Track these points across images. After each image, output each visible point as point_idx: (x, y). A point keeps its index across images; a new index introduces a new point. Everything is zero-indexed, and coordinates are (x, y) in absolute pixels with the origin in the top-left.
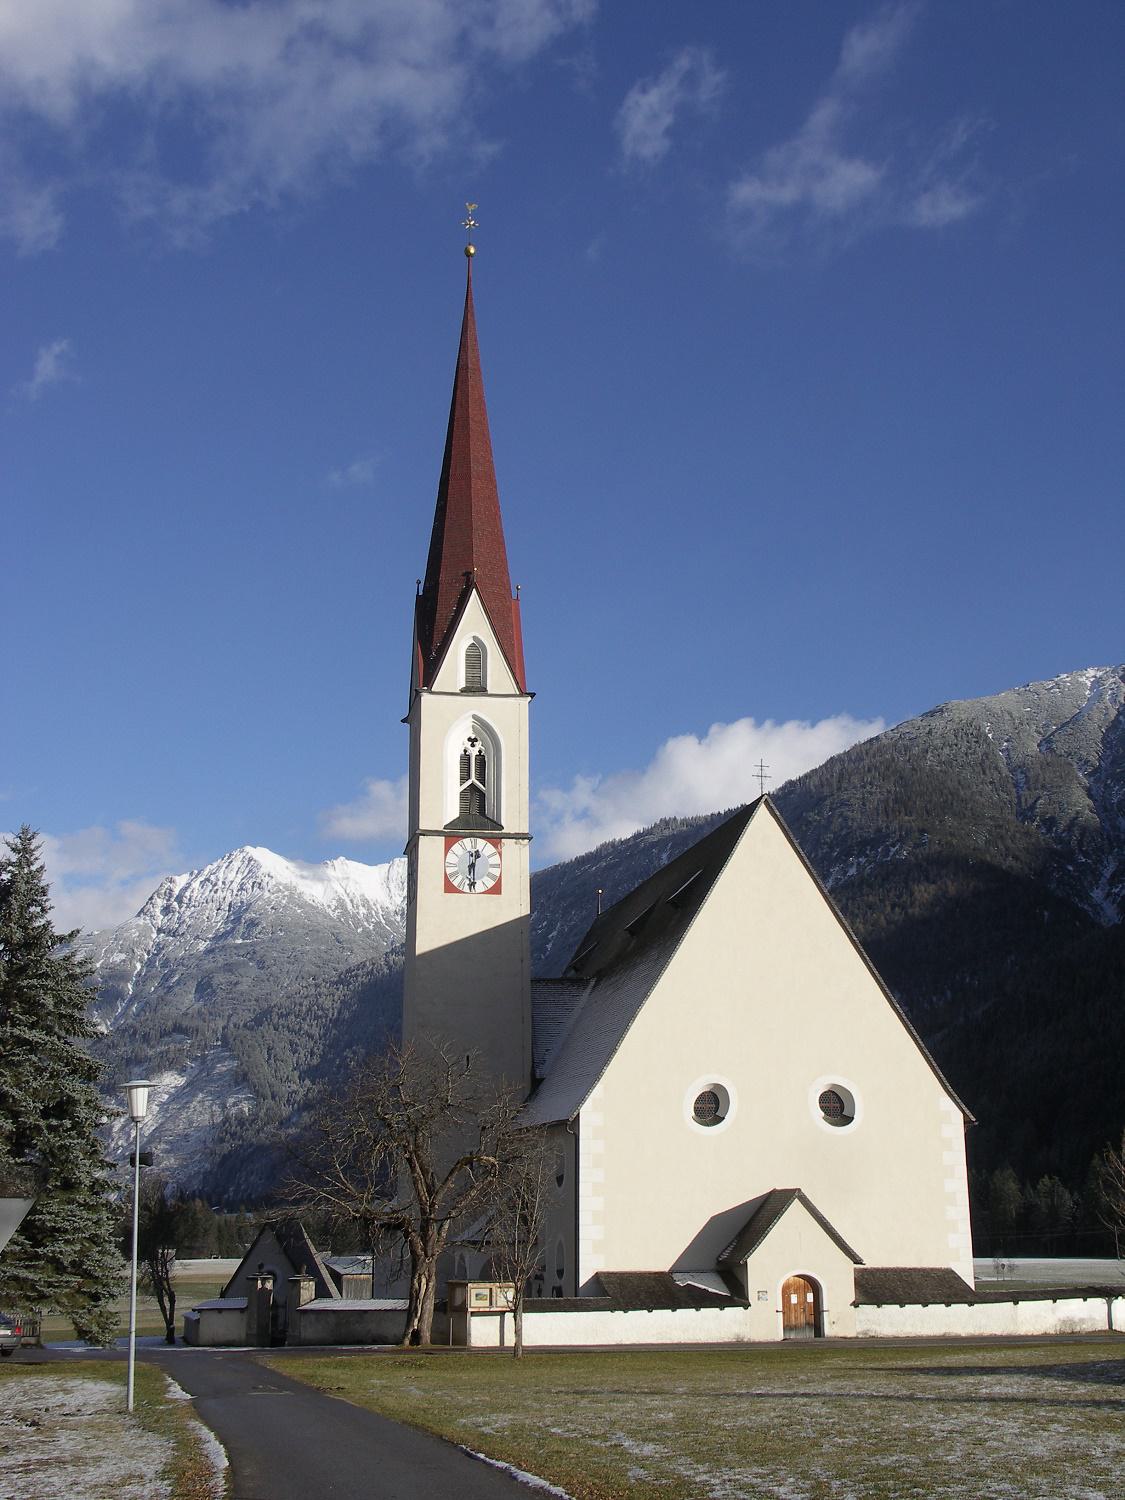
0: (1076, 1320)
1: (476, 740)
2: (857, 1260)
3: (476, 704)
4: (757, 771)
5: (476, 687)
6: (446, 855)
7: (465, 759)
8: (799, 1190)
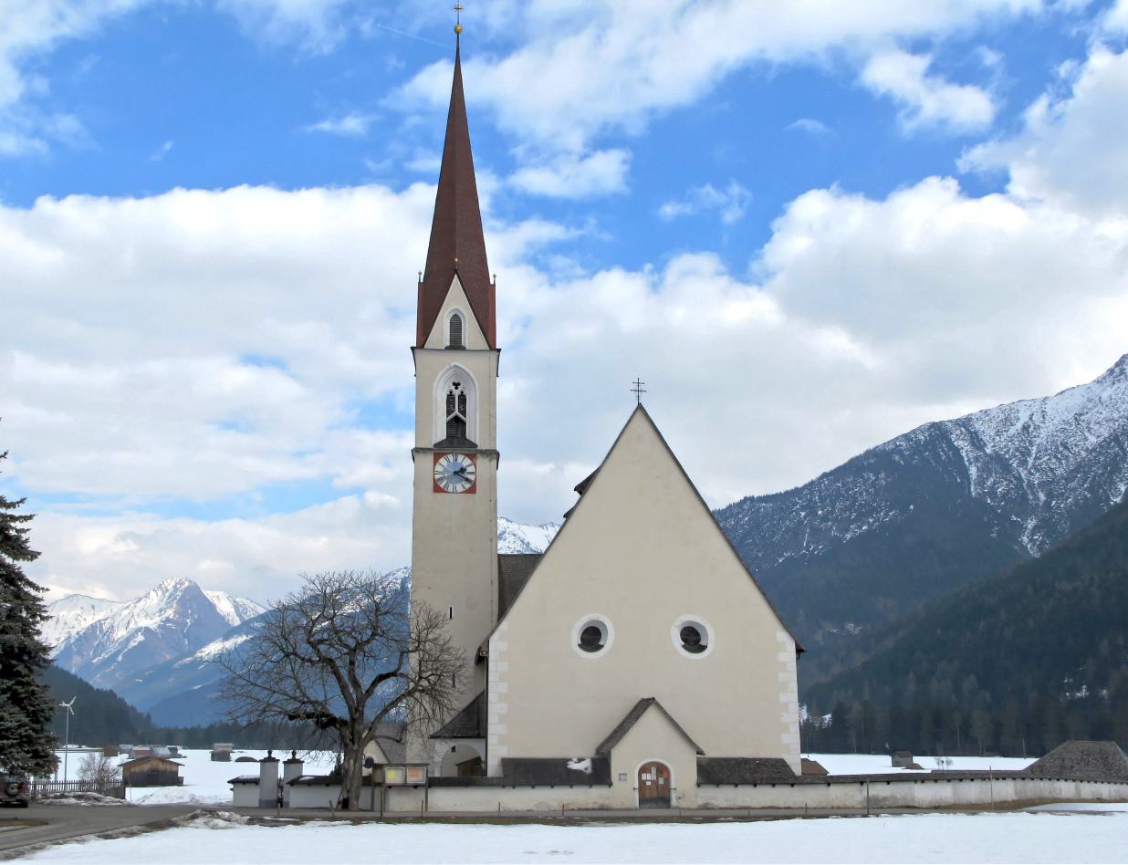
0: (880, 797)
2: (700, 752)
3: (457, 359)
4: (635, 387)
7: (450, 397)
8: (653, 699)
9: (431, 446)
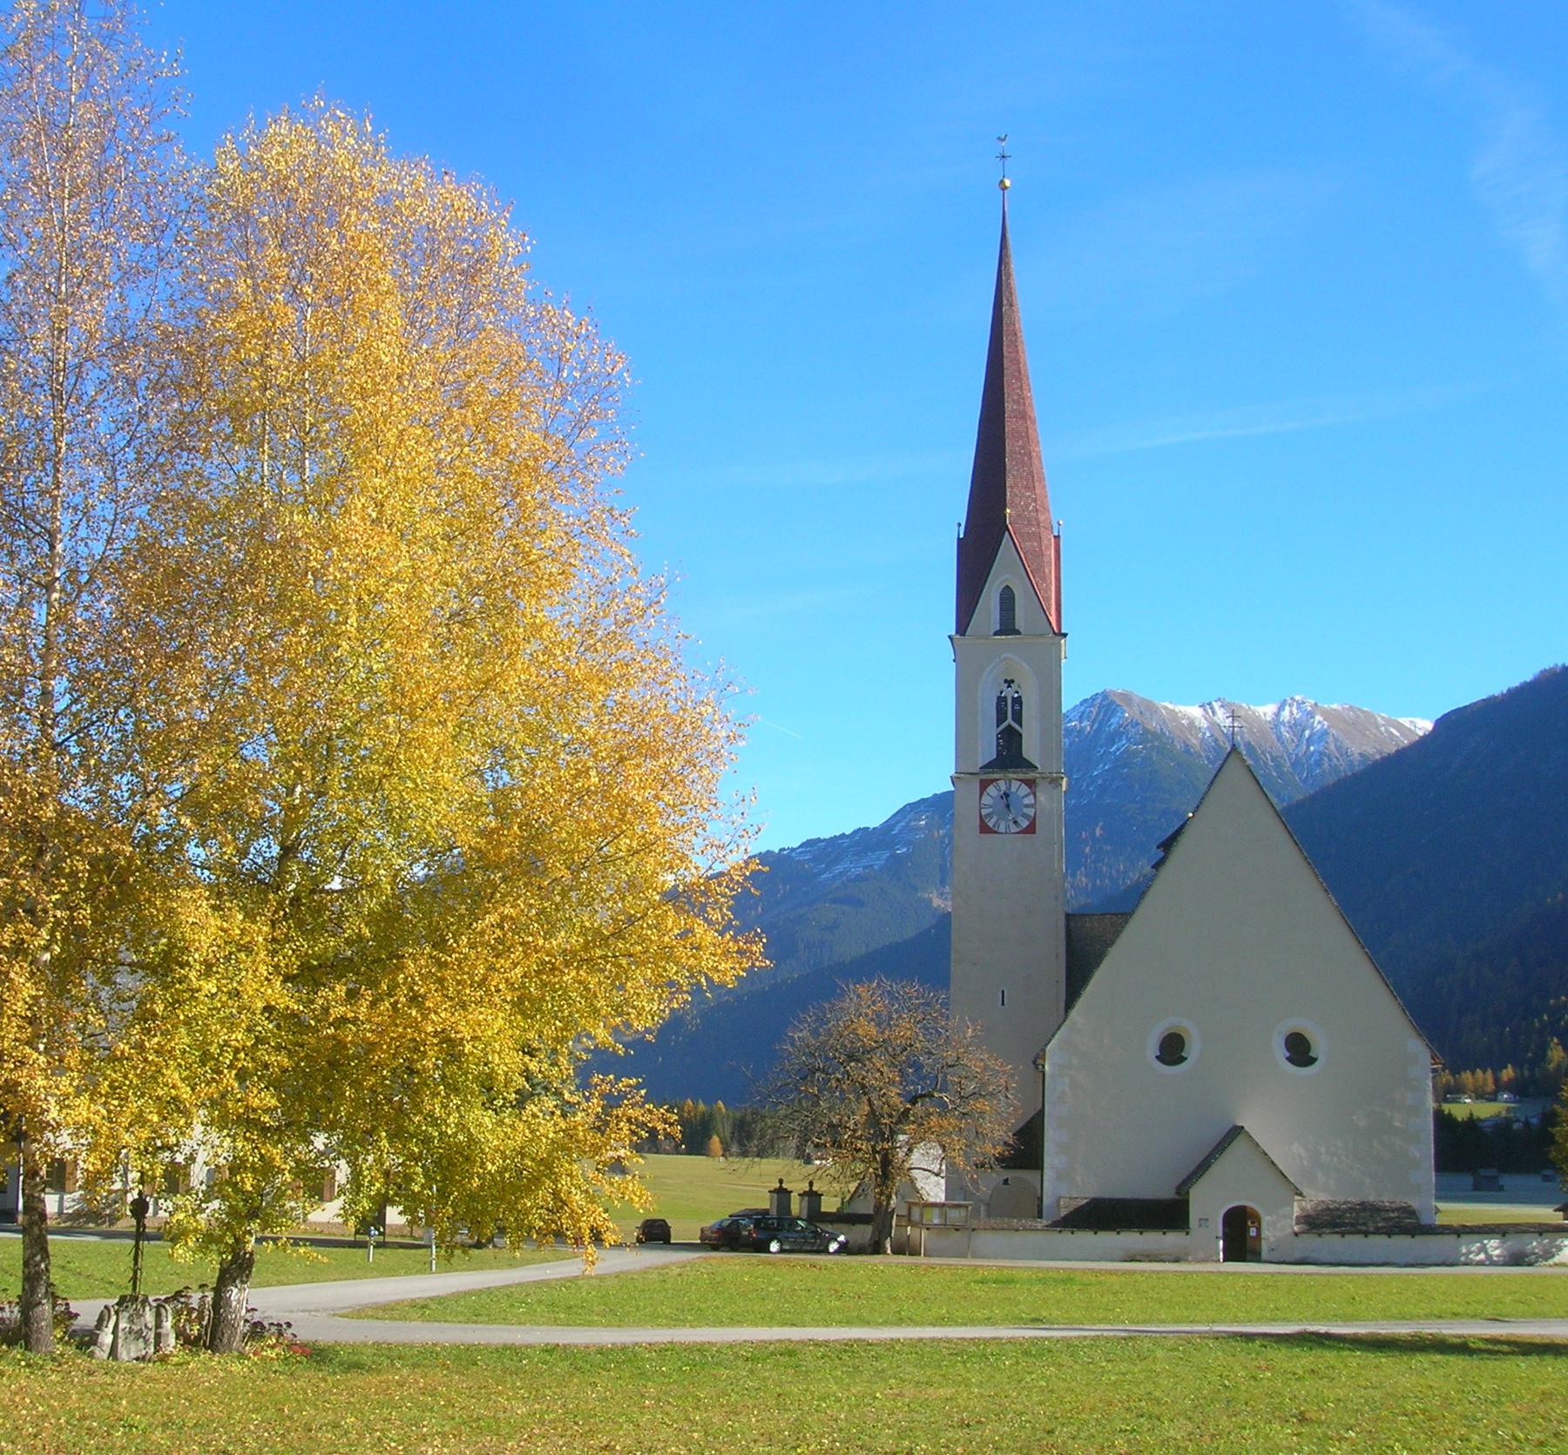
7: (1001, 700)
9: (977, 770)
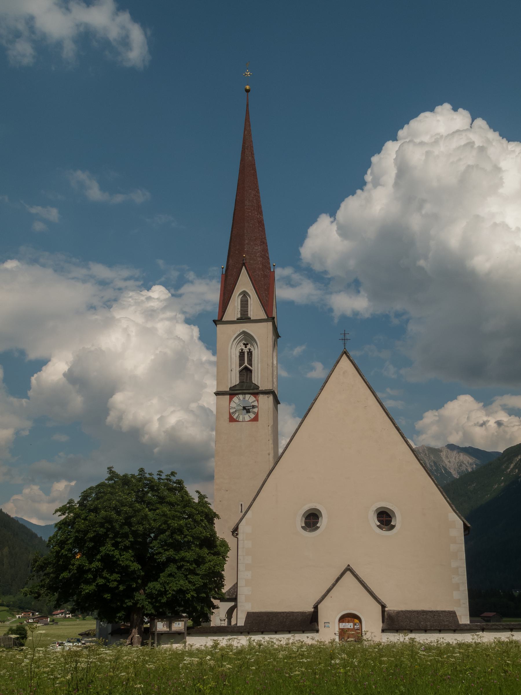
1: (247, 344)
4: (342, 337)
5: (244, 318)
6: (230, 403)
